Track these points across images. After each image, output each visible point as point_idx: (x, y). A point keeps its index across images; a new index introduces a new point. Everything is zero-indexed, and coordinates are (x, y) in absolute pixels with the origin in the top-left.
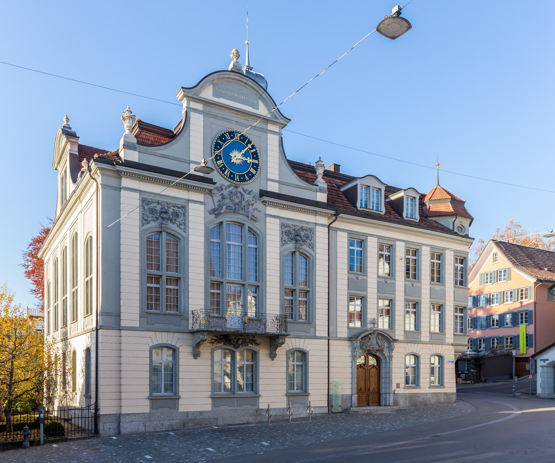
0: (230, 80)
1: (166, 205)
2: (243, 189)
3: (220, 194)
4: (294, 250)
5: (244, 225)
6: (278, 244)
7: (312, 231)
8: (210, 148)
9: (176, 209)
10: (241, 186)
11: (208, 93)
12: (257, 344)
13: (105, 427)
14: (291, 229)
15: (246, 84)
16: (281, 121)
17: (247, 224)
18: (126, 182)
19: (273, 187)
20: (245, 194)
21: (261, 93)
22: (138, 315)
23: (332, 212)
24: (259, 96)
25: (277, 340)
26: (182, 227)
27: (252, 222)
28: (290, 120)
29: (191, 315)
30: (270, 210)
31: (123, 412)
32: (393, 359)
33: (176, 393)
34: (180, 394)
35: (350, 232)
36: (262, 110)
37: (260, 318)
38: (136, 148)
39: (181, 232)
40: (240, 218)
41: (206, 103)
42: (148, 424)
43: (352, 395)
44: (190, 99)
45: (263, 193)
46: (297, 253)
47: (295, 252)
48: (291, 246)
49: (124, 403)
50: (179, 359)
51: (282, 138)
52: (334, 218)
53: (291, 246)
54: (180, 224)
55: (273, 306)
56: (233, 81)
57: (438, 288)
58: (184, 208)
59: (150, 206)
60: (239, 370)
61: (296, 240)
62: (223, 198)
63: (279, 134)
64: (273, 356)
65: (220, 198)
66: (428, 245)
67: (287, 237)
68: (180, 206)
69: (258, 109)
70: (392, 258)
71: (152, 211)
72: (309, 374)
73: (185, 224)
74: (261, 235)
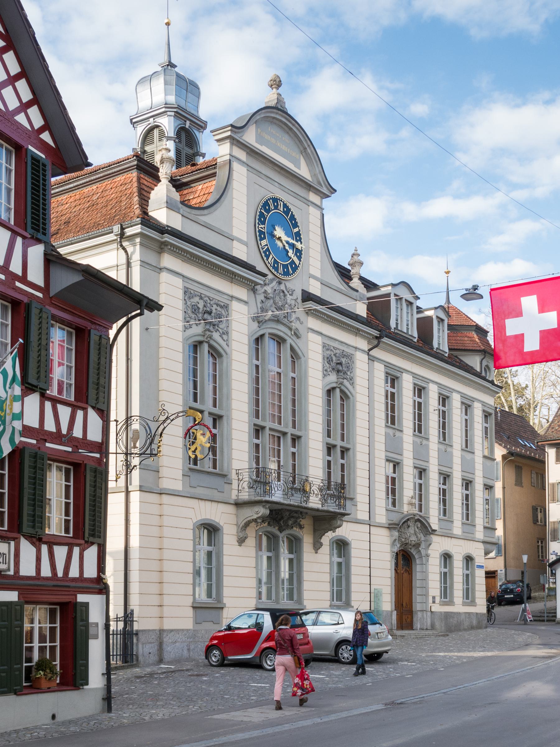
0: (275, 120)
1: (209, 301)
2: (286, 287)
3: (263, 291)
4: (334, 385)
5: (284, 341)
6: (320, 375)
7: (350, 357)
8: (253, 220)
9: (219, 308)
10: (283, 282)
11: (250, 137)
12: (301, 527)
13: (144, 649)
14: (333, 354)
15: (291, 129)
16: (325, 190)
17: (289, 341)
18: (168, 261)
19: (315, 289)
20: (288, 296)
21: (307, 146)
22: (181, 473)
23: (376, 333)
24: (302, 149)
25: (334, 522)
26: (225, 337)
27: (294, 338)
28: (335, 191)
29: (234, 476)
30: (313, 323)
31: (165, 628)
32: (430, 559)
33: (219, 598)
34: (225, 600)
35: (387, 365)
36: (304, 171)
37: (298, 485)
38: (179, 209)
39: (223, 344)
40: (281, 330)
41: (252, 152)
42: (192, 647)
43: (392, 612)
44: (235, 142)
45: (307, 297)
46: (206, 347)
47: (201, 343)
48: (333, 378)
49: (167, 611)
50: (223, 544)
51: (323, 214)
52: (376, 342)
53: (197, 330)
54: (224, 333)
55: (315, 469)
56: (277, 122)
57: (468, 456)
58: (226, 307)
59: (192, 300)
60: (549, 567)
61: (338, 371)
62: (266, 298)
63: (321, 208)
64: (317, 546)
65: (263, 298)
66: (320, 334)
67: (328, 365)
68: (222, 304)
69: (299, 168)
70: (425, 407)
71: (195, 309)
72: (225, 579)
73: (227, 333)
74: (303, 359)
